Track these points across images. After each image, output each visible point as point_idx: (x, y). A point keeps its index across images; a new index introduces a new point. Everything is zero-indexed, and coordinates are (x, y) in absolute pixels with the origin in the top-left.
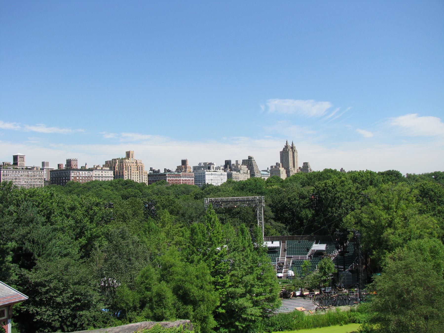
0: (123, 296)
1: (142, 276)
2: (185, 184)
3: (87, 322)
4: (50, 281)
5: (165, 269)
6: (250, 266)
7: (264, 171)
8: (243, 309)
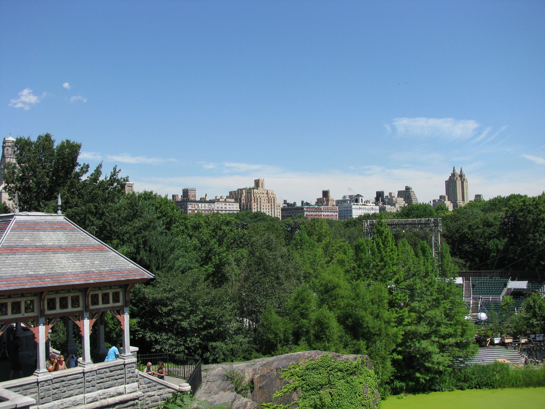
0: (271, 324)
1: (296, 299)
3: (222, 357)
4: (172, 300)
5: (327, 291)
6: (435, 297)
8: (427, 355)
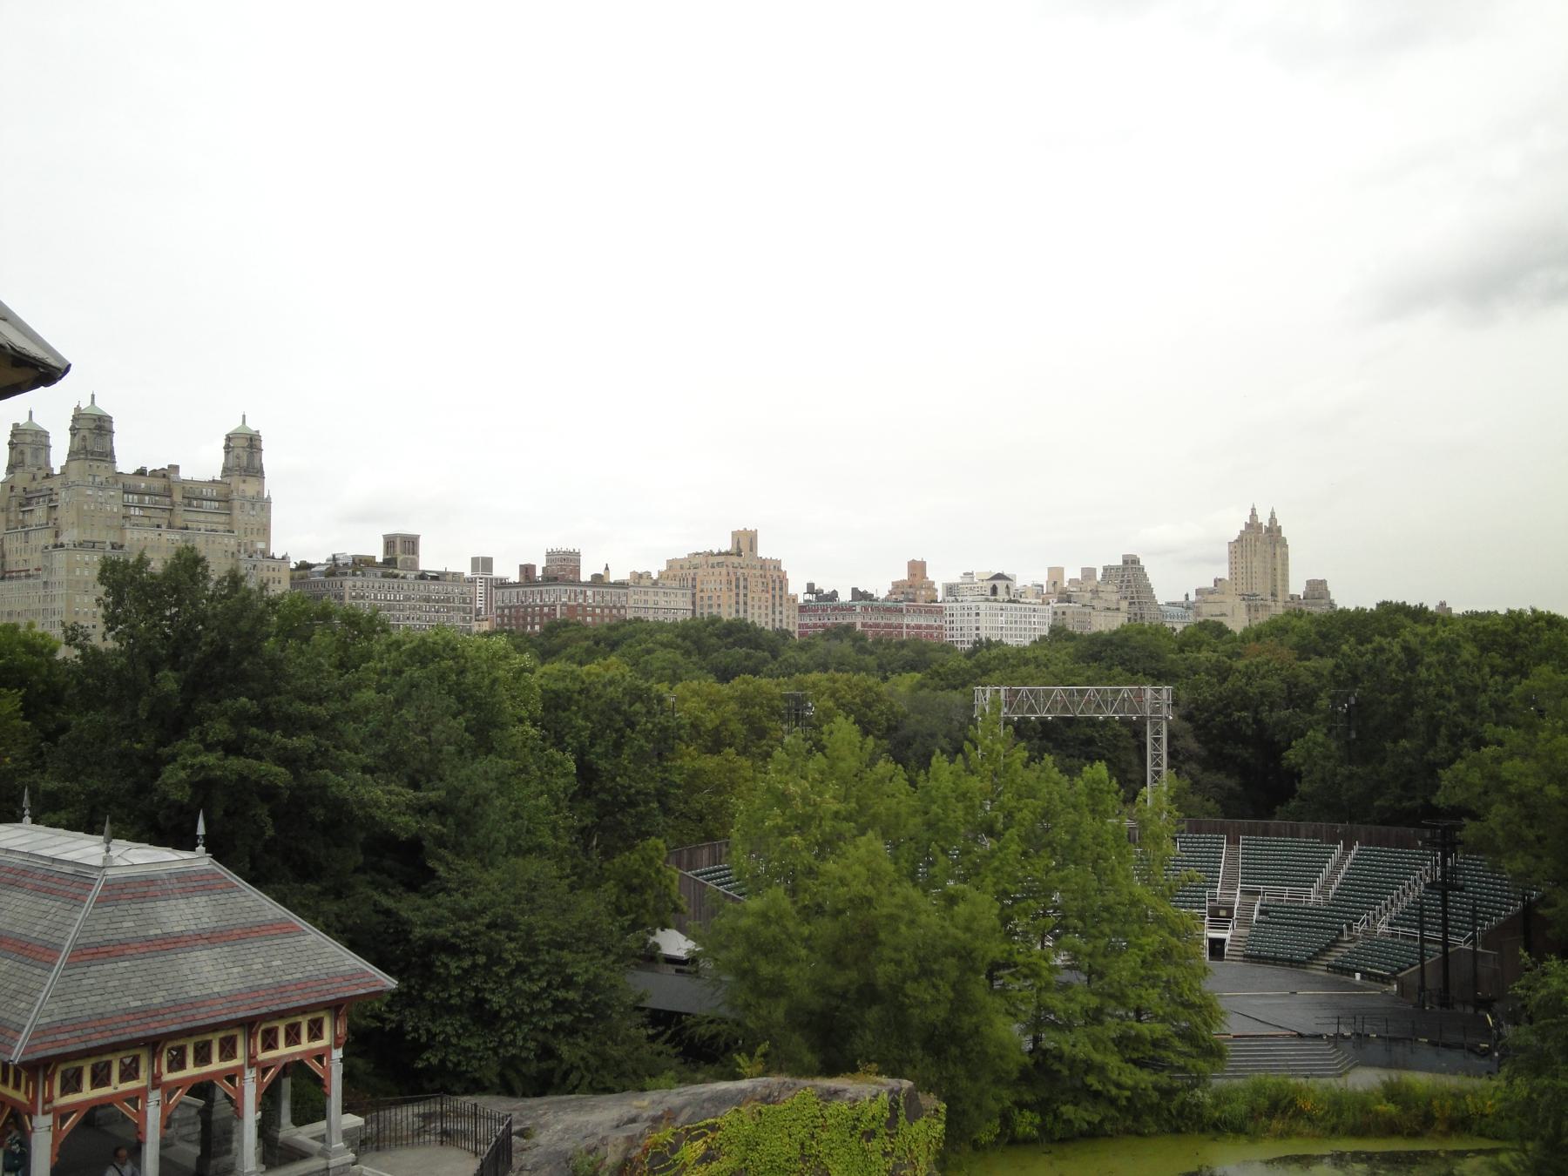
2: (917, 639)
7: (1174, 604)
